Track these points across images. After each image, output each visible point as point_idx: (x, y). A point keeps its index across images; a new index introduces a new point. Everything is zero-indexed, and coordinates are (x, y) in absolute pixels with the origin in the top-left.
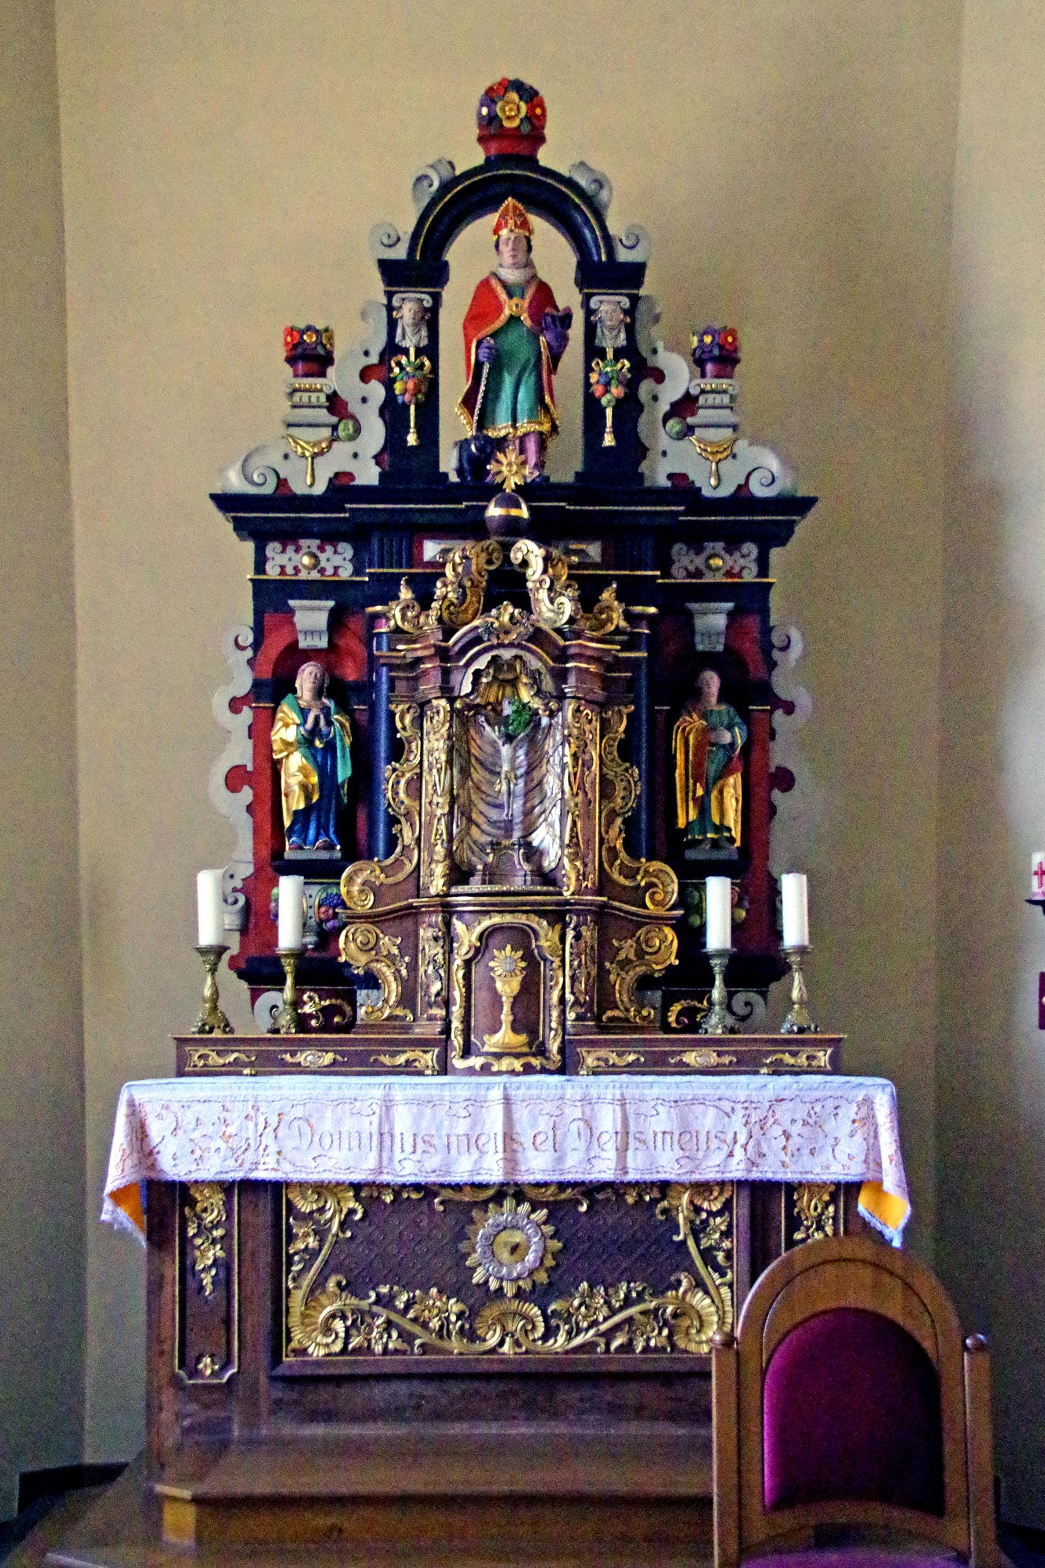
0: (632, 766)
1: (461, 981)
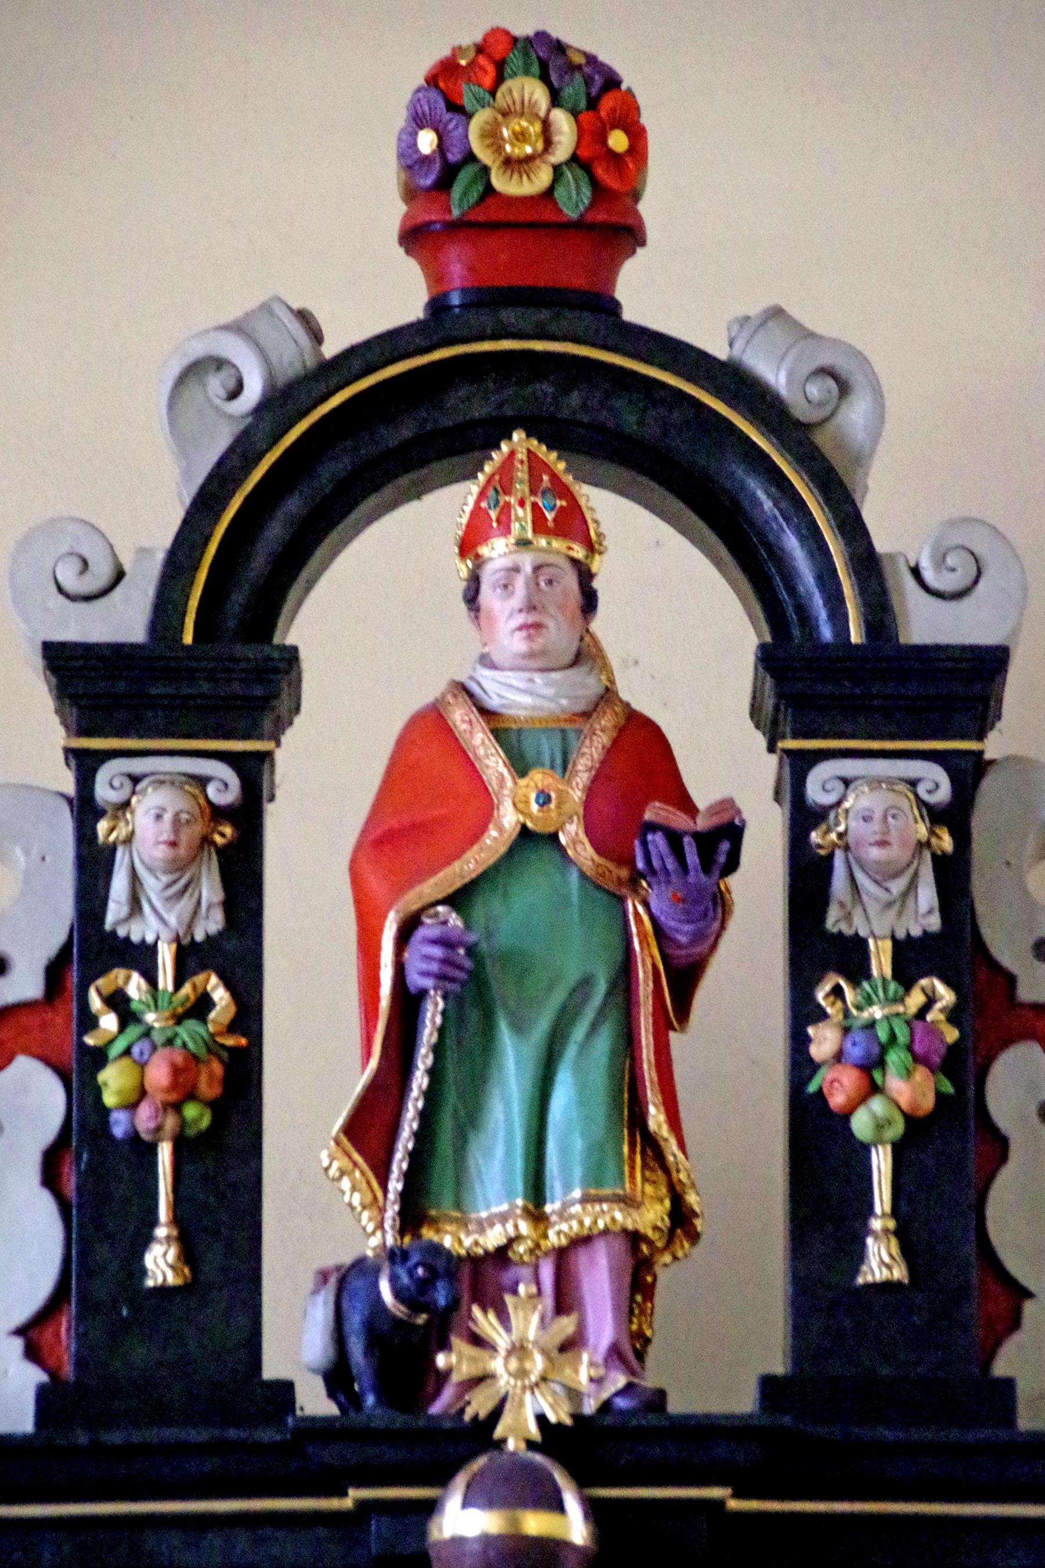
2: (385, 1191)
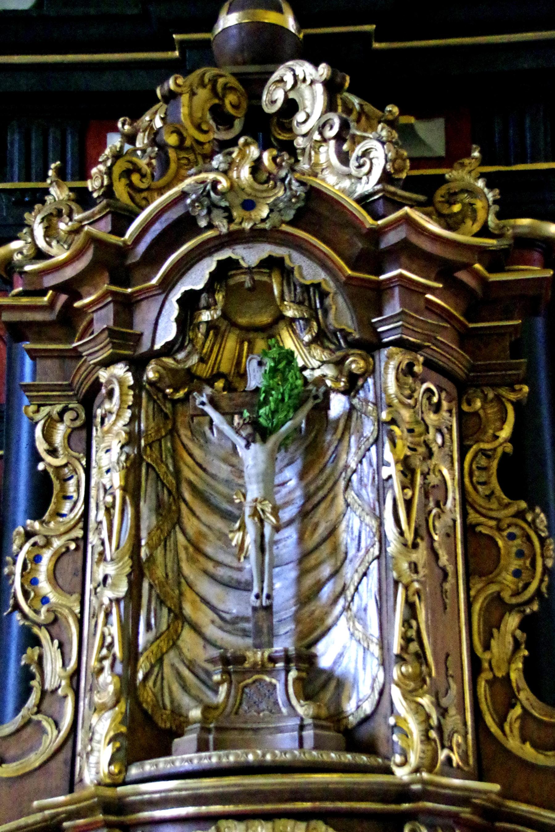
0: (531, 508)
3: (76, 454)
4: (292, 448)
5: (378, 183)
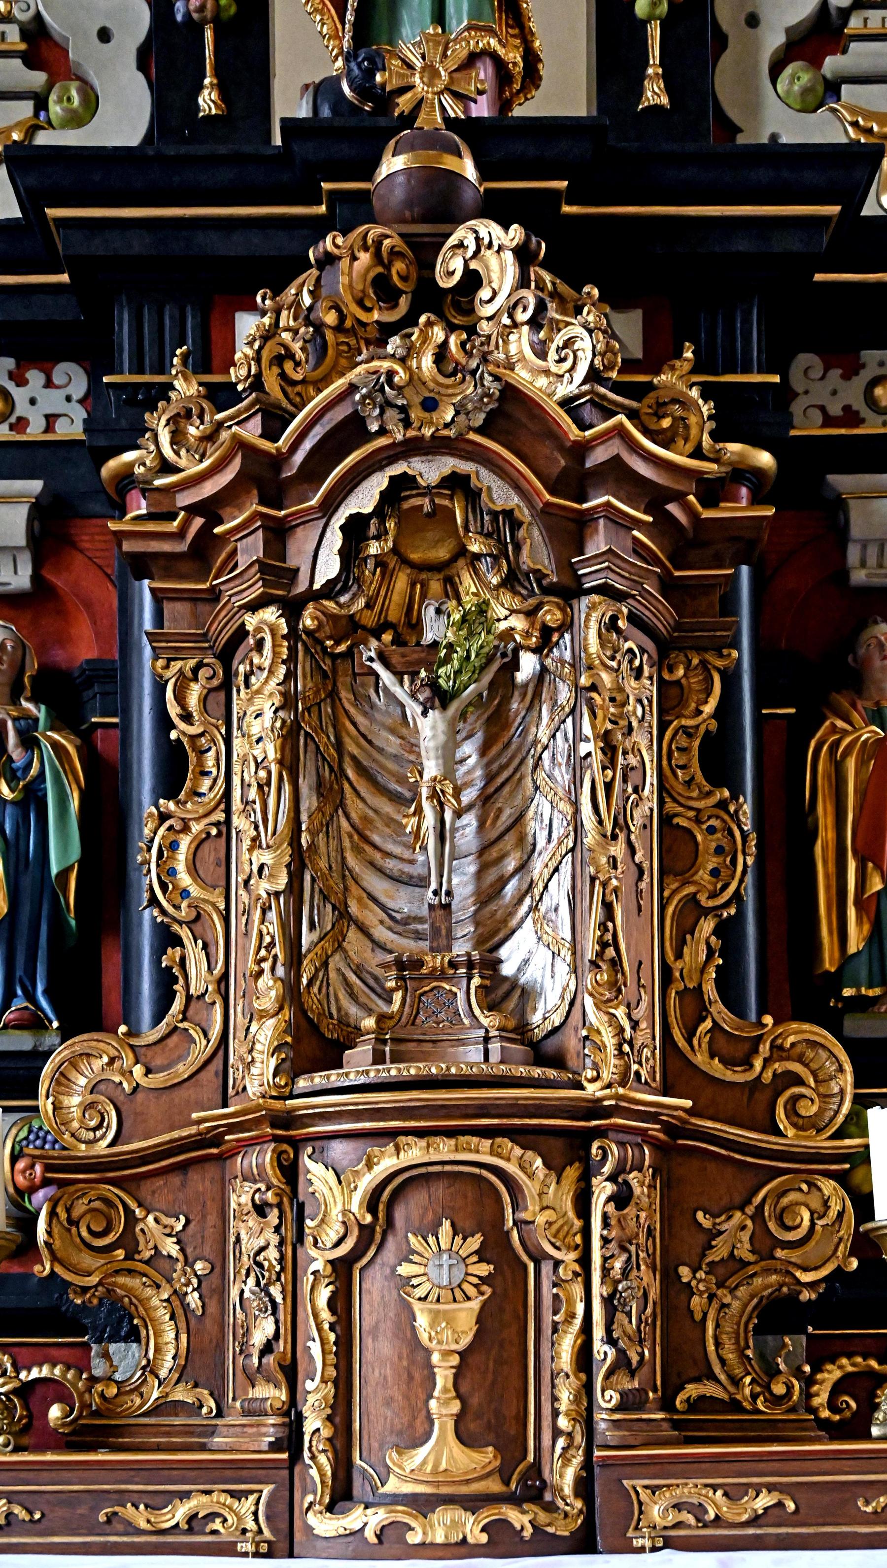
1: (326, 1315)
2: (343, 24)
3: (214, 721)
4: (471, 719)
5: (584, 383)
